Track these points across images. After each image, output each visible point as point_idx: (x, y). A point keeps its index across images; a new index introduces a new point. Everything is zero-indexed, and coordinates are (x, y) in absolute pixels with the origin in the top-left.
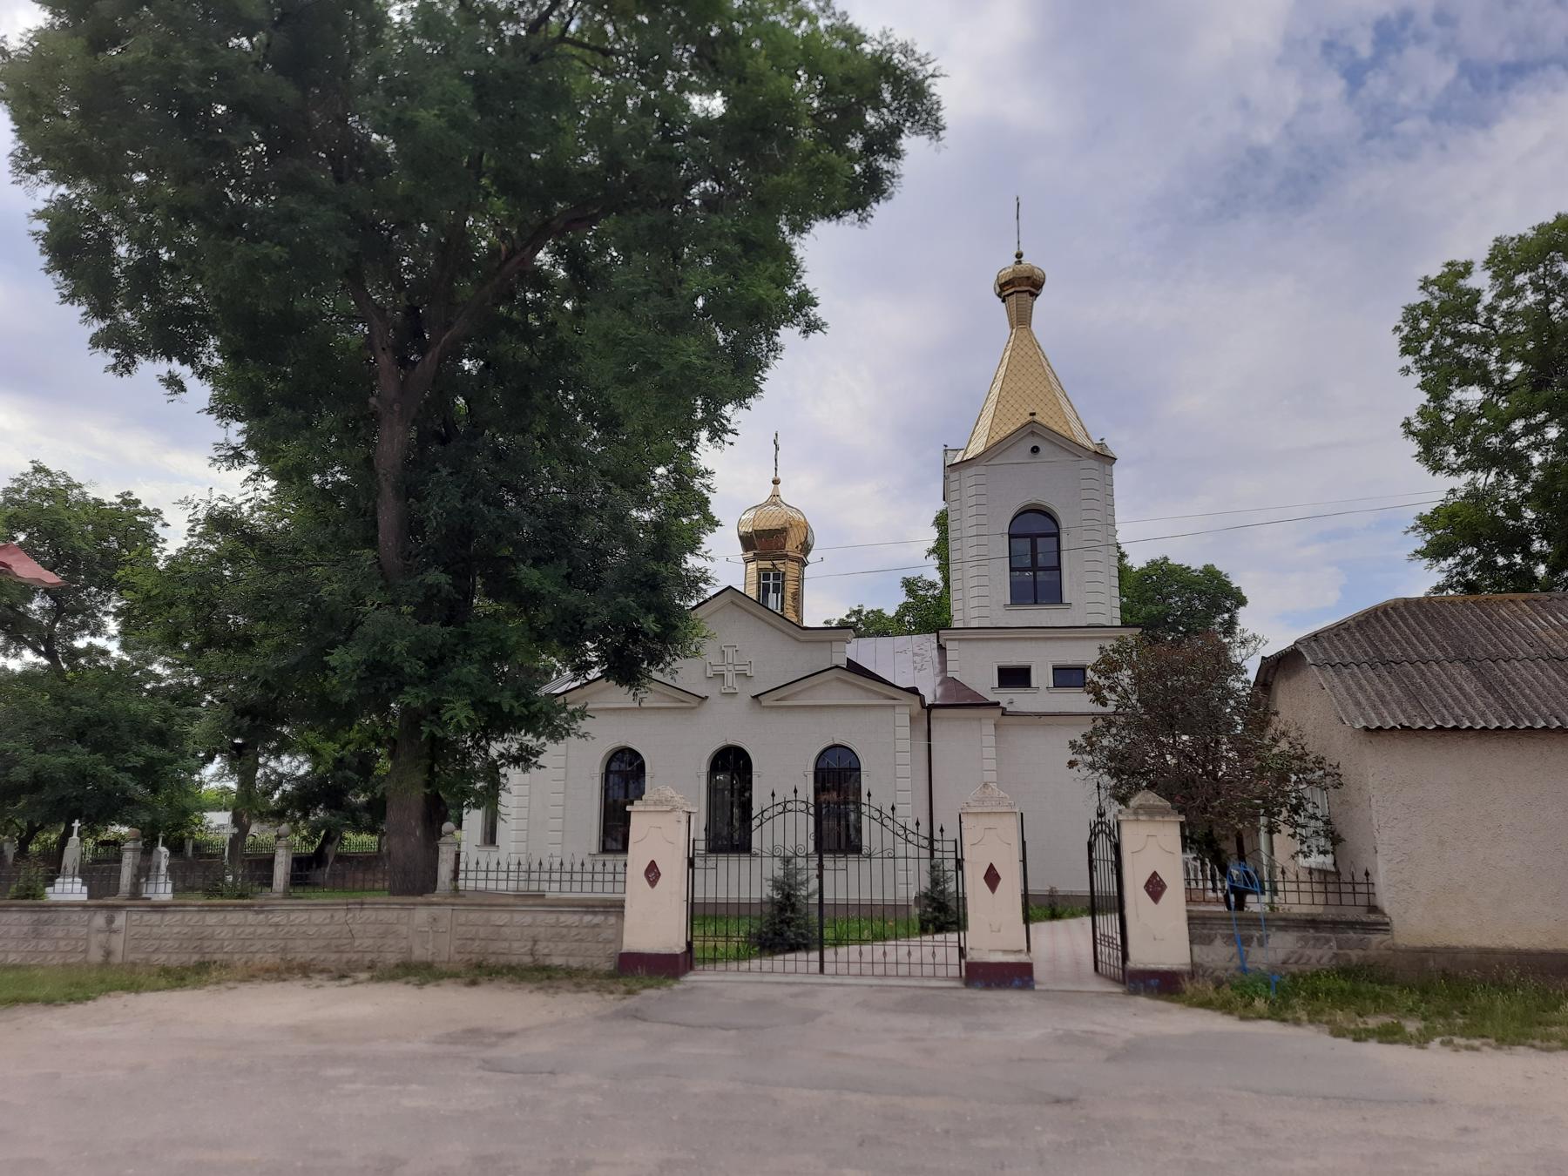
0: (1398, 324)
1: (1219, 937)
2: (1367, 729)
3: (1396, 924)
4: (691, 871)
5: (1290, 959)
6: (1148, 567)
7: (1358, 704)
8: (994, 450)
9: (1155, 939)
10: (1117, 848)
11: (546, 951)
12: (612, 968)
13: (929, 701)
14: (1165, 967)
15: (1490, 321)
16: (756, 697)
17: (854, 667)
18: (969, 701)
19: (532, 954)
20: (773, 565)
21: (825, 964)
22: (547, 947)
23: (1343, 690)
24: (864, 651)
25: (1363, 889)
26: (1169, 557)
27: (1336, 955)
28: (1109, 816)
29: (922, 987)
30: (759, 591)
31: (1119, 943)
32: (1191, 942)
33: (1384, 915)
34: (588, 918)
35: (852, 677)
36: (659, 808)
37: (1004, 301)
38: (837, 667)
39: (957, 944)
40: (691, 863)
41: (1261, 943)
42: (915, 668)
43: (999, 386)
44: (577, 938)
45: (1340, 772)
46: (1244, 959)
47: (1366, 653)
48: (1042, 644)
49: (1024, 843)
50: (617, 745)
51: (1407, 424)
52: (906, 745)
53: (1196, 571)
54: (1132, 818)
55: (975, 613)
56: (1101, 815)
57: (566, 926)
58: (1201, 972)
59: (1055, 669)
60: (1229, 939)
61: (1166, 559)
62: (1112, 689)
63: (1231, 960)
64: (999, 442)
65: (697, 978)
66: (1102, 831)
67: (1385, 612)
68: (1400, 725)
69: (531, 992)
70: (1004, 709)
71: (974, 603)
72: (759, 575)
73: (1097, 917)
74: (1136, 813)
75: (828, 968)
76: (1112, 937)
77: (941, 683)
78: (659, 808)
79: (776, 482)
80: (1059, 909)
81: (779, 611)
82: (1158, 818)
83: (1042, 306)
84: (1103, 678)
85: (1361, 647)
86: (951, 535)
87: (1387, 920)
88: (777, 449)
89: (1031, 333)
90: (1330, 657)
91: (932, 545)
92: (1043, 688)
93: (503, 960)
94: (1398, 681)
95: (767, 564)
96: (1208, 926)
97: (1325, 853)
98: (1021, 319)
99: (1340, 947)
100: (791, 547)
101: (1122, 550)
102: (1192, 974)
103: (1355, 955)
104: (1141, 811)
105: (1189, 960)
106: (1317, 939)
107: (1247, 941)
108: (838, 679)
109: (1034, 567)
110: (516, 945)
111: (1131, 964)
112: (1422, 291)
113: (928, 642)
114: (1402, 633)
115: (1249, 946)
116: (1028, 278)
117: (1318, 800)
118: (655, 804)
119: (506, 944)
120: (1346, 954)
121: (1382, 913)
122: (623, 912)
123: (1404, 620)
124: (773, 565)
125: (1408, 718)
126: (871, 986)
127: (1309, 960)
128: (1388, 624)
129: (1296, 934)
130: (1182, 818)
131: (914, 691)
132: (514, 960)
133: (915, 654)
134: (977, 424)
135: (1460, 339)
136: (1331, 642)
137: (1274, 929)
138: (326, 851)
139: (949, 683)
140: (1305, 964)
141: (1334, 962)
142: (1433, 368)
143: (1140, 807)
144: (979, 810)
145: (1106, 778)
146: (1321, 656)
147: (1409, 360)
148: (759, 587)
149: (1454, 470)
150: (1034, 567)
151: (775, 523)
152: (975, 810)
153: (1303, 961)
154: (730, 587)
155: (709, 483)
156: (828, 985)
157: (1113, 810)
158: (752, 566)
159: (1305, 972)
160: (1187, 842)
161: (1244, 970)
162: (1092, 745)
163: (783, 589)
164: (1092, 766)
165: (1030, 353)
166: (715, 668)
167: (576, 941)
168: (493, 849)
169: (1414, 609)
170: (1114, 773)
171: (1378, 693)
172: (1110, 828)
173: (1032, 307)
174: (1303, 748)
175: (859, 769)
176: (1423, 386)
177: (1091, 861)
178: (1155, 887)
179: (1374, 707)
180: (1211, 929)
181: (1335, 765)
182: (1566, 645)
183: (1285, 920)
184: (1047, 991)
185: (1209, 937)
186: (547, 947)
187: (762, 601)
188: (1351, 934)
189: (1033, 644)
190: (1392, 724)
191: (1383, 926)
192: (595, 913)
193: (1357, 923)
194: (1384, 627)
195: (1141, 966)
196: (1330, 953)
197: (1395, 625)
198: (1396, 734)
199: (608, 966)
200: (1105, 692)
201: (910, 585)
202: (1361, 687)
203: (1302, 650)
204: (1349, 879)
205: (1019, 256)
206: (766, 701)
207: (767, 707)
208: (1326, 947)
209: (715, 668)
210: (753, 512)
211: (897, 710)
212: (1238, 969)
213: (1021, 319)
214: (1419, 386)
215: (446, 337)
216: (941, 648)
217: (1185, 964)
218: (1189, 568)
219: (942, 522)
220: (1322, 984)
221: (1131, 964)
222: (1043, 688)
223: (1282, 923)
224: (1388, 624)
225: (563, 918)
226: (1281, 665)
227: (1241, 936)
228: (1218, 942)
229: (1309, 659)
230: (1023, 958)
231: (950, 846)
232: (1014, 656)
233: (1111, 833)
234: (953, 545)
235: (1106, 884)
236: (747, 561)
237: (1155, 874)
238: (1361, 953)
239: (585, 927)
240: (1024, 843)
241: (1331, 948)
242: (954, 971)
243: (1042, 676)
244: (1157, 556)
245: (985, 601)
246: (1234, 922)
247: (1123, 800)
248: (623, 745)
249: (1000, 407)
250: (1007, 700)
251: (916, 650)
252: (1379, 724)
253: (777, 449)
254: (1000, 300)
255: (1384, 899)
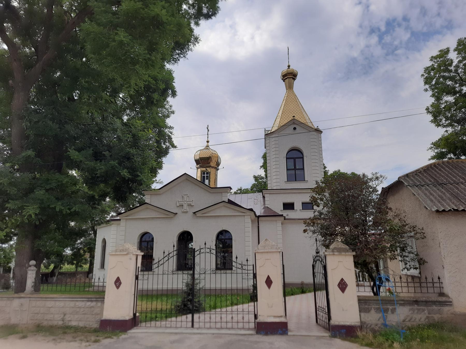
0: (423, 74)
1: (373, 309)
2: (437, 211)
3: (455, 302)
4: (137, 281)
5: (406, 319)
6: (334, 173)
7: (432, 201)
8: (282, 128)
9: (343, 310)
10: (325, 268)
11: (69, 319)
12: (98, 327)
13: (258, 214)
14: (348, 324)
15: (456, 71)
16: (194, 213)
17: (230, 202)
18: (272, 214)
19: (63, 321)
20: (206, 169)
21: (194, 323)
22: (70, 317)
23: (423, 195)
24: (237, 199)
25: (438, 285)
26: (340, 170)
27: (428, 317)
28: (321, 253)
29: (236, 334)
30: (201, 178)
31: (327, 311)
32: (360, 311)
33: (449, 297)
34: (89, 303)
35: (229, 205)
36: (122, 253)
37: (284, 81)
38: (224, 201)
39: (254, 313)
40: (137, 278)
41: (393, 311)
42: (254, 204)
43: (283, 108)
44: (83, 313)
45: (423, 232)
46: (385, 320)
47: (430, 181)
48: (298, 195)
49: (283, 266)
50: (144, 231)
51: (427, 109)
52: (250, 234)
53: (349, 174)
54: (331, 253)
55: (275, 184)
56: (317, 253)
57: (79, 307)
58: (365, 326)
59: (303, 203)
60: (378, 310)
61: (339, 170)
62: (322, 200)
63: (379, 320)
64: (282, 126)
65: (134, 331)
66: (318, 260)
67: (431, 167)
68: (453, 209)
69: (48, 342)
70: (285, 217)
71: (275, 181)
72: (201, 173)
73: (316, 293)
74: (333, 251)
75: (196, 325)
76: (323, 308)
77: (263, 208)
78: (122, 253)
79: (208, 142)
80: (305, 289)
81: (208, 185)
82: (343, 253)
83: (296, 83)
84: (317, 195)
85: (427, 179)
86: (268, 162)
87: (451, 300)
88: (208, 131)
89: (293, 91)
90: (415, 183)
91: (262, 164)
92: (298, 210)
93: (50, 323)
94: (448, 191)
95: (204, 169)
96: (368, 304)
97: (416, 268)
98: (290, 87)
99: (429, 314)
100: (213, 164)
101: (325, 165)
102: (361, 327)
103: (436, 317)
104: (335, 250)
105: (359, 320)
106: (419, 310)
107: (386, 311)
108: (224, 206)
109: (295, 169)
110: (56, 316)
111: (333, 322)
112: (431, 61)
113: (259, 195)
114: (444, 173)
115: (387, 313)
116: (292, 73)
117: (413, 245)
118: (120, 251)
119: (52, 316)
120: (432, 317)
121: (447, 296)
122: (104, 300)
123: (444, 169)
124: (206, 169)
125: (456, 206)
126: (213, 334)
127: (415, 320)
128: (437, 170)
129: (409, 307)
130: (354, 253)
131: (251, 210)
132: (55, 323)
133: (254, 199)
134: (275, 121)
135: (445, 78)
136: (414, 177)
137: (398, 305)
138: (55, 271)
139: (266, 208)
140: (414, 321)
141: (427, 320)
142: (436, 88)
143: (335, 248)
144: (263, 251)
145: (320, 237)
146: (411, 182)
147: (427, 86)
148: (201, 177)
149: (445, 126)
150: (295, 169)
151: (206, 155)
152: (261, 251)
153: (413, 320)
154: (185, 174)
155: (172, 131)
156: (195, 334)
157: (322, 251)
158: (199, 170)
159: (414, 325)
160: (356, 264)
161: (386, 325)
162: (314, 223)
163: (210, 177)
164: (314, 232)
165: (293, 98)
166: (180, 203)
167: (83, 314)
168: (103, 270)
169: (447, 164)
170: (324, 235)
171: (439, 196)
172: (321, 258)
173: (293, 83)
174: (405, 222)
175: (232, 239)
176: (433, 96)
177: (314, 273)
178: (343, 286)
179: (439, 202)
180: (369, 305)
181: (421, 228)
182: (465, 197)
183: (403, 300)
184: (294, 335)
185: (368, 309)
186: (70, 317)
187: (203, 182)
188: (434, 307)
189: (295, 195)
190: (449, 208)
191: (448, 303)
192: (92, 301)
193: (437, 301)
194: (435, 171)
195: (337, 323)
196: (425, 317)
197: (440, 170)
198: (450, 213)
199: (96, 325)
200: (319, 201)
201: (256, 178)
202: (431, 194)
203: (402, 180)
204: (431, 281)
205: (289, 66)
206: (198, 214)
207: (198, 216)
208: (423, 313)
209: (180, 203)
210: (199, 151)
211: (246, 217)
212: (382, 324)
213: (290, 87)
214: (431, 96)
215: (45, 57)
216: (264, 197)
217: (358, 322)
218: (347, 173)
219: (265, 157)
220: (425, 333)
221: (333, 322)
222: (298, 210)
223: (402, 302)
224: (437, 170)
225: (77, 303)
226: (388, 191)
227: (383, 308)
228: (373, 311)
229: (406, 184)
230: (283, 320)
231: (251, 268)
232: (288, 199)
233: (322, 260)
234: (268, 165)
235: (320, 279)
236: (198, 168)
237: (342, 280)
238: (440, 316)
239: (87, 307)
240: (283, 266)
241: (425, 314)
242: (252, 325)
243: (298, 206)
244: (336, 169)
245: (278, 180)
246: (380, 302)
247: (327, 247)
248: (146, 231)
249: (283, 115)
250: (286, 214)
251: (255, 198)
252: (443, 209)
253: (208, 131)
254: (283, 81)
255: (448, 290)
